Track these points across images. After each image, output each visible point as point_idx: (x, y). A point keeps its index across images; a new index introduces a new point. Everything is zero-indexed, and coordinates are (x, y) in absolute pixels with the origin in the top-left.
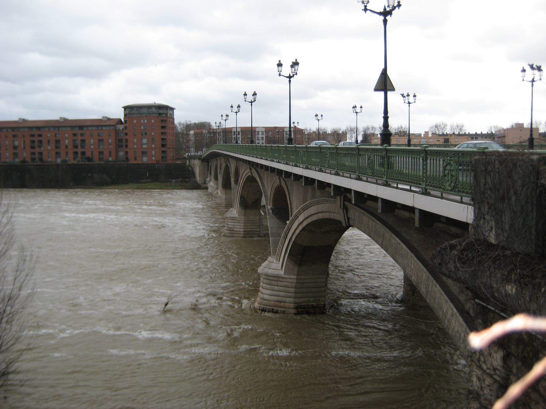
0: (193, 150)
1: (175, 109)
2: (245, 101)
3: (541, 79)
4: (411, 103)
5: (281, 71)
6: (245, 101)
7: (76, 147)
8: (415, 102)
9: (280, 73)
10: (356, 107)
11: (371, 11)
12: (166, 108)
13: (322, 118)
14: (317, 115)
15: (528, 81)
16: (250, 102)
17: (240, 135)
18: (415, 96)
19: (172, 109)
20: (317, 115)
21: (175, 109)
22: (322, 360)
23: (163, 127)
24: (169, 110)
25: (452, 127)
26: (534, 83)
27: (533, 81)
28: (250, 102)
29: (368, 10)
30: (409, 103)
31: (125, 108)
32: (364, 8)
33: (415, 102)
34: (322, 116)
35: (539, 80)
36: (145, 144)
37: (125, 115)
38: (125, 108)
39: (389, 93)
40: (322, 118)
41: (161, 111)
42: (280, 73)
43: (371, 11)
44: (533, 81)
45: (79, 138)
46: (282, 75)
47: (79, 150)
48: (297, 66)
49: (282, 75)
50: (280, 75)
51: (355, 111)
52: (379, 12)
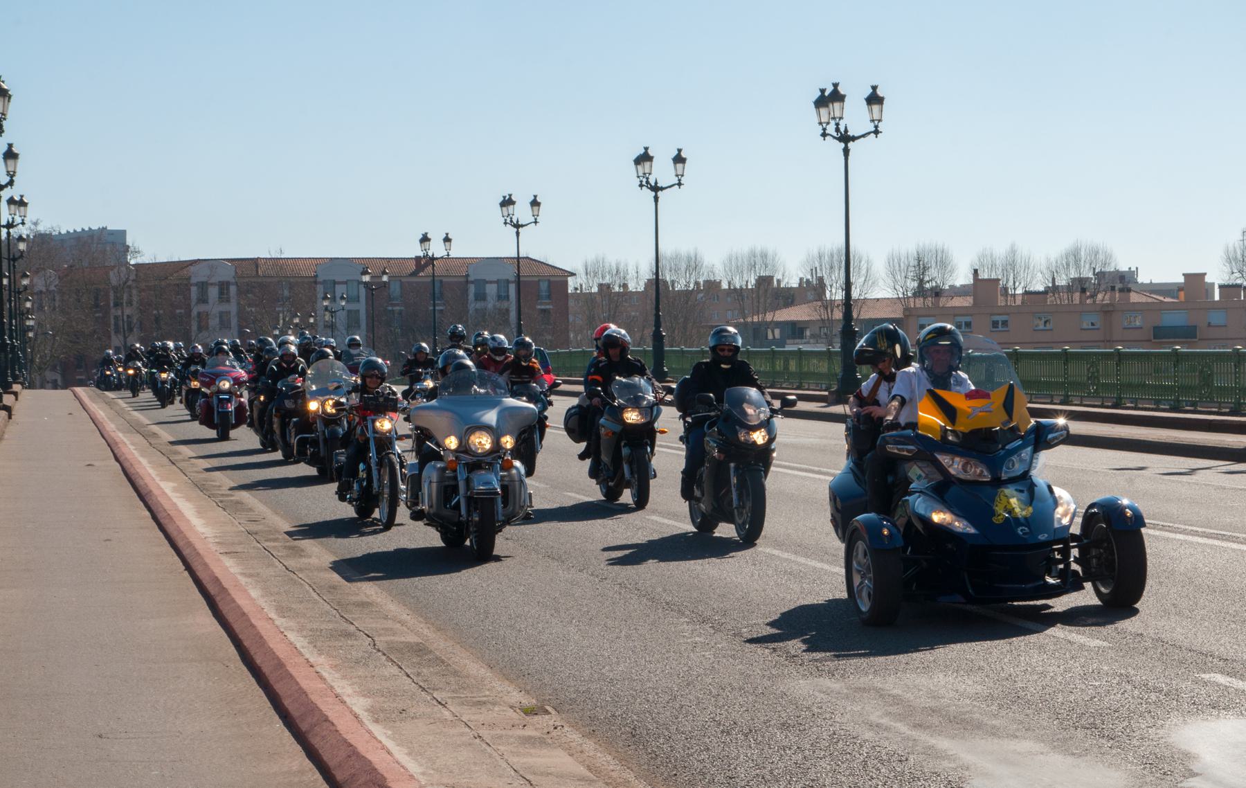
8: (876, 132)
13: (536, 216)
14: (507, 202)
20: (644, 158)
30: (845, 138)
35: (677, 186)
40: (536, 216)
51: (831, 129)
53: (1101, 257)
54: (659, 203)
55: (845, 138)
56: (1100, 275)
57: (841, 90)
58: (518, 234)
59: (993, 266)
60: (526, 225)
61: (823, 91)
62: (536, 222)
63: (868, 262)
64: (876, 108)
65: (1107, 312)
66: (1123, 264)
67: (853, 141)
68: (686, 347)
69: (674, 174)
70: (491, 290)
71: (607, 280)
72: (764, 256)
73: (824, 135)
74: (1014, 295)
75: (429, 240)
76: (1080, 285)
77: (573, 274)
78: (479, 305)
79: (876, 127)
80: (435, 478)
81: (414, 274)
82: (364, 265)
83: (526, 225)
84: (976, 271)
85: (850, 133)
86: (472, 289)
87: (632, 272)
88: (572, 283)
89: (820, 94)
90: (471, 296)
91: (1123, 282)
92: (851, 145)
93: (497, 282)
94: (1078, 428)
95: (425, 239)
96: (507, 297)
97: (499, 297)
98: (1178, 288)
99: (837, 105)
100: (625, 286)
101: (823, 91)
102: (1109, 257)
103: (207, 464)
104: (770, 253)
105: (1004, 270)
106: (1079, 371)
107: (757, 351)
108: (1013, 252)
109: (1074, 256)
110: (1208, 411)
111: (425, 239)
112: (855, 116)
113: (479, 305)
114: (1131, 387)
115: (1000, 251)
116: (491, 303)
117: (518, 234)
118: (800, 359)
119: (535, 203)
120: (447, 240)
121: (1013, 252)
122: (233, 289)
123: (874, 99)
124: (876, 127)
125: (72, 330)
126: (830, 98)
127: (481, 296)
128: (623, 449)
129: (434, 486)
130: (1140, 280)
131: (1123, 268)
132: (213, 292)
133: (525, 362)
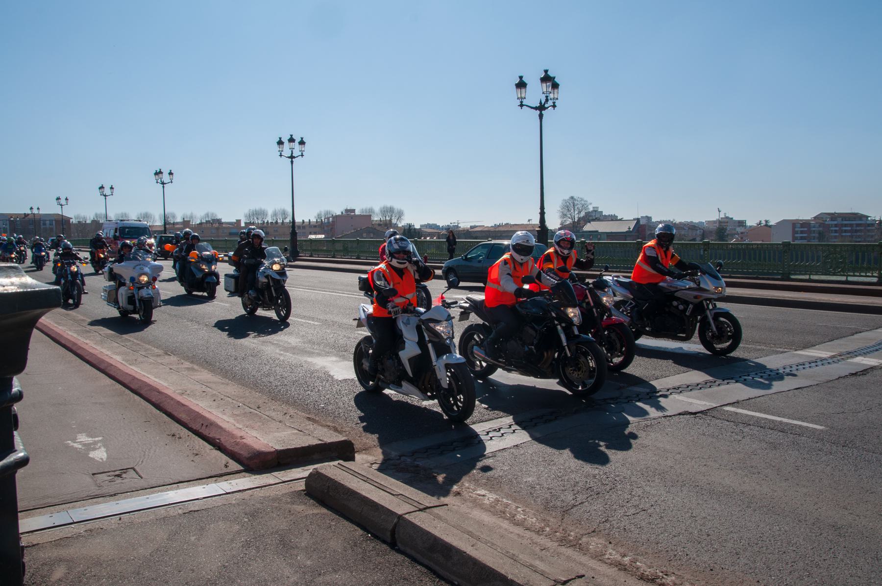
8: (172, 182)
10: (161, 172)
13: (67, 203)
14: (102, 188)
15: (287, 157)
17: (118, 232)
20: (102, 188)
22: (743, 433)
25: (275, 214)
28: (536, 108)
29: (525, 105)
30: (163, 183)
32: (519, 104)
33: (112, 195)
34: (112, 188)
35: (301, 157)
40: (67, 203)
46: (527, 106)
49: (527, 106)
50: (522, 105)
51: (159, 181)
52: (535, 106)
53: (214, 215)
54: (293, 165)
55: (163, 183)
56: (213, 220)
57: (162, 171)
58: (163, 187)
59: (187, 217)
62: (172, 182)
63: (154, 216)
64: (171, 176)
65: (217, 229)
66: (219, 217)
67: (536, 107)
68: (360, 238)
69: (114, 190)
70: (48, 222)
71: (81, 220)
72: (125, 214)
73: (157, 182)
74: (192, 225)
75: (33, 209)
76: (207, 222)
77: (72, 218)
78: (44, 226)
80: (124, 293)
81: (24, 218)
82: (11, 215)
83: (297, 157)
84: (184, 219)
85: (165, 182)
86: (42, 222)
87: (88, 218)
88: (71, 220)
89: (290, 137)
90: (42, 224)
91: (219, 221)
92: (165, 185)
93: (50, 220)
94: (730, 291)
95: (31, 208)
96: (52, 225)
97: (50, 225)
98: (235, 223)
99: (161, 175)
100: (85, 222)
101: (156, 171)
102: (216, 215)
103: (279, 476)
104: (127, 213)
105: (190, 218)
107: (870, 244)
108: (192, 214)
109: (207, 215)
110: (772, 278)
111: (31, 208)
112: (166, 178)
113: (44, 226)
114: (314, 250)
115: (189, 213)
116: (48, 226)
117: (163, 187)
120: (38, 209)
121: (192, 214)
123: (171, 173)
126: (158, 173)
127: (45, 224)
128: (483, 321)
129: (124, 297)
130: (222, 221)
131: (219, 218)
133: (21, 237)
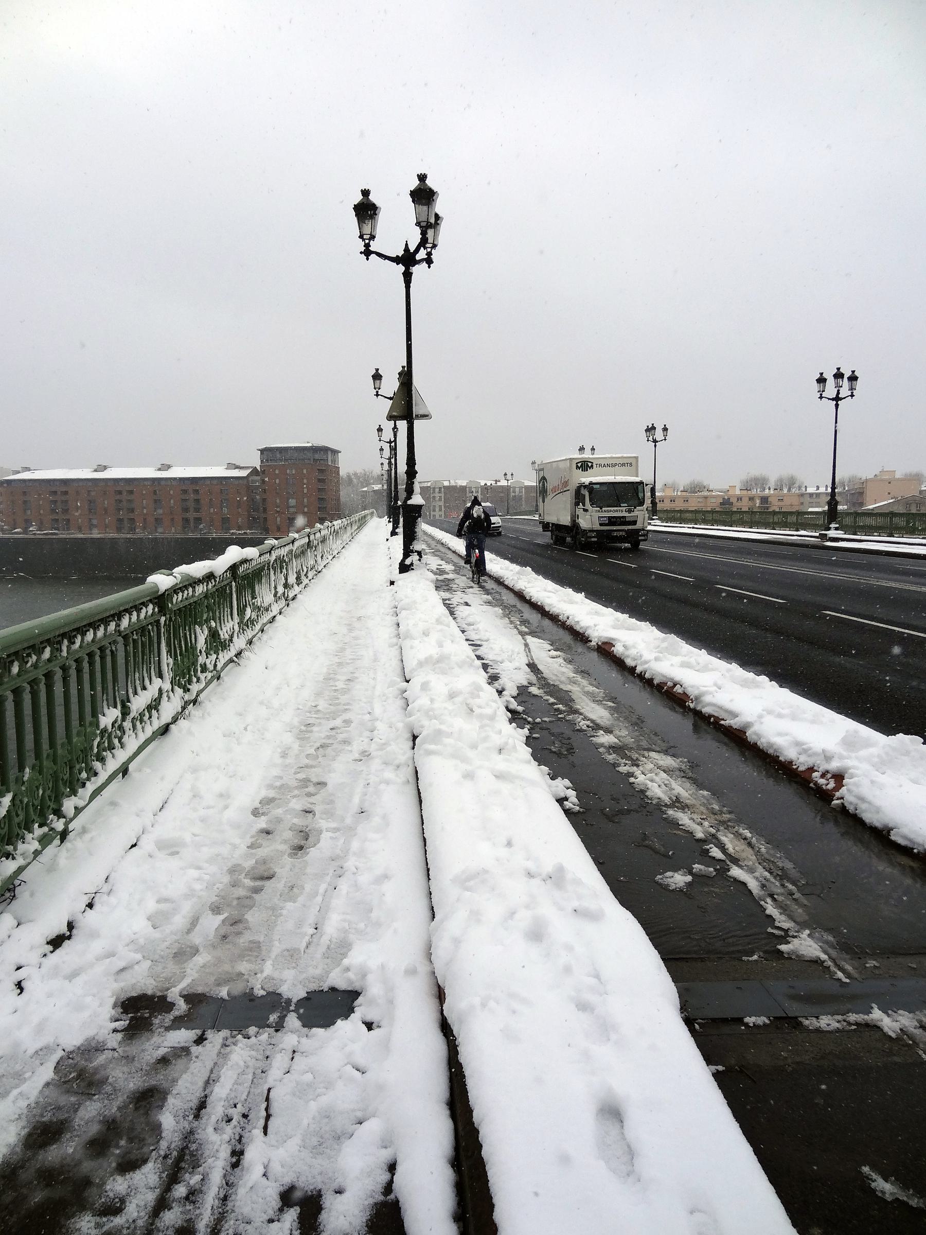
0: (440, 506)
1: (340, 452)
2: (380, 440)
3: (852, 396)
4: (657, 442)
5: (379, 389)
6: (380, 440)
7: (186, 510)
8: (665, 440)
9: (377, 392)
11: (379, 255)
12: (325, 450)
15: (829, 399)
16: (387, 442)
18: (665, 429)
19: (335, 452)
21: (340, 452)
23: (321, 481)
24: (329, 453)
26: (839, 402)
27: (837, 399)
28: (387, 442)
30: (655, 441)
31: (262, 451)
32: (363, 249)
33: (665, 440)
36: (293, 507)
37: (262, 461)
38: (262, 451)
39: (417, 423)
41: (317, 456)
42: (377, 392)
43: (379, 255)
44: (837, 399)
45: (192, 496)
46: (382, 396)
47: (191, 515)
48: (378, 381)
49: (382, 396)
51: (651, 439)
55: (655, 441)
60: (845, 398)
61: (648, 426)
70: (517, 490)
73: (648, 440)
79: (852, 393)
83: (845, 398)
86: (512, 489)
101: (648, 426)
106: (700, 516)
112: (659, 435)
118: (855, 518)
119: (665, 429)
122: (443, 489)
124: (852, 393)
125: (234, 584)
126: (651, 429)
127: (514, 492)
132: (437, 490)
